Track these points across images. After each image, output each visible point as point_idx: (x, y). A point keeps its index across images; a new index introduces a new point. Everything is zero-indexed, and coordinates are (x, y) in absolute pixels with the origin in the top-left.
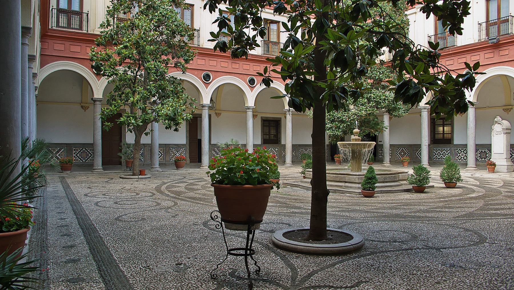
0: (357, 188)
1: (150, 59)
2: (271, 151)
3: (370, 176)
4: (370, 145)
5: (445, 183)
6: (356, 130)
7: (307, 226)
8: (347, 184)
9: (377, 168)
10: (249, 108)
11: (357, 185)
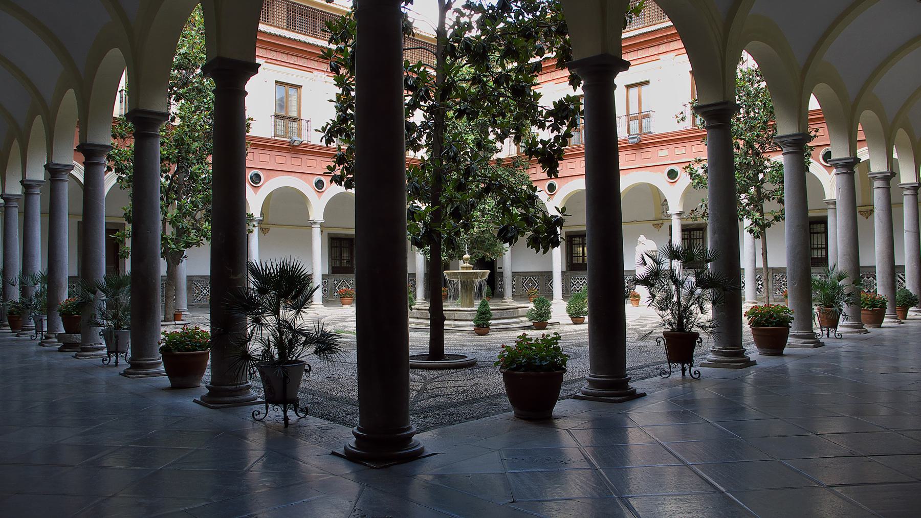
0: (470, 325)
1: (195, 161)
2: (344, 284)
3: (484, 310)
4: (483, 274)
5: (572, 319)
6: (467, 256)
7: (427, 352)
8: (457, 322)
9: (493, 305)
10: (315, 223)
11: (469, 323)
